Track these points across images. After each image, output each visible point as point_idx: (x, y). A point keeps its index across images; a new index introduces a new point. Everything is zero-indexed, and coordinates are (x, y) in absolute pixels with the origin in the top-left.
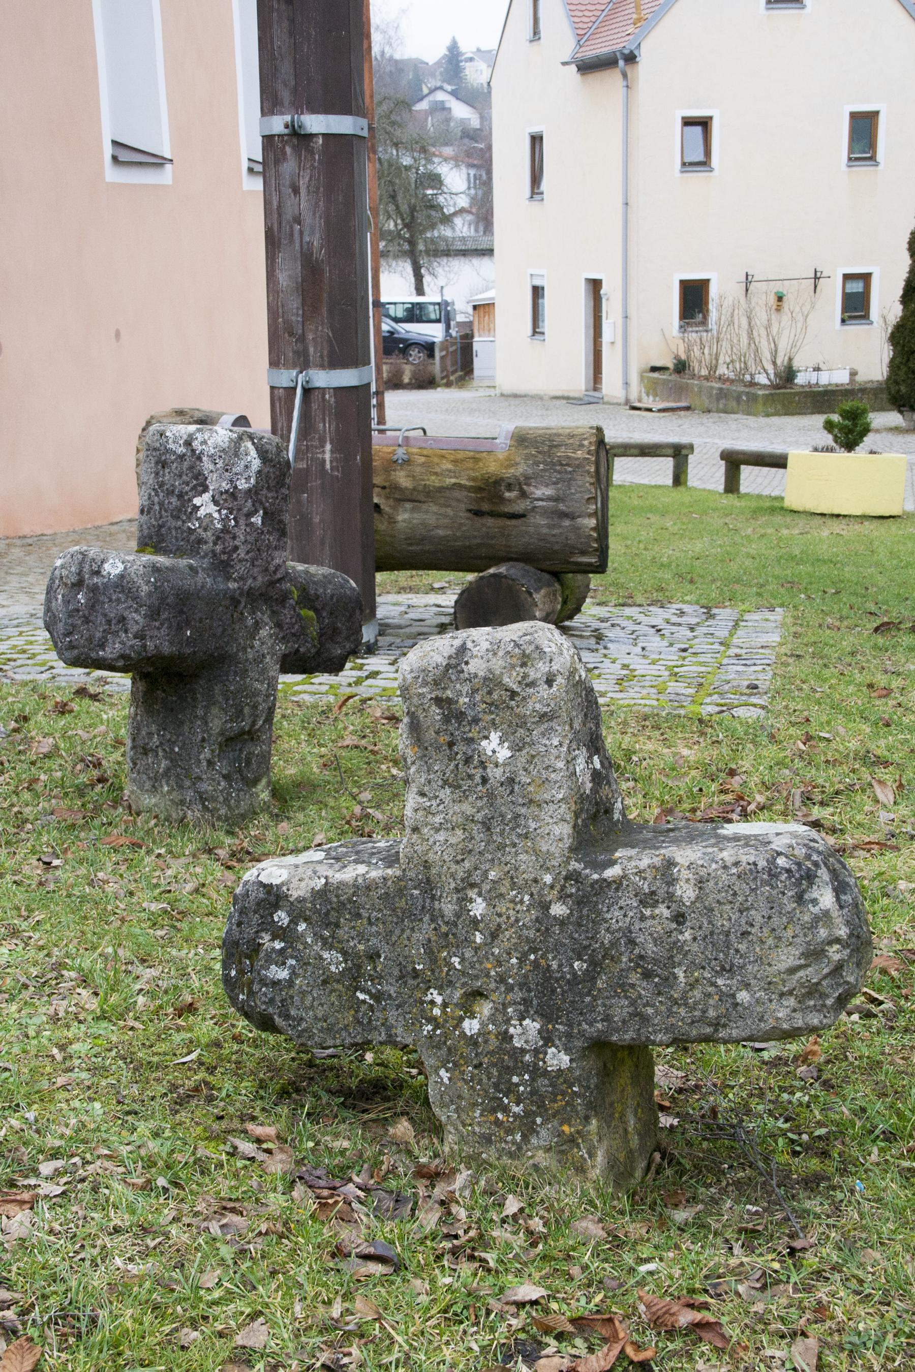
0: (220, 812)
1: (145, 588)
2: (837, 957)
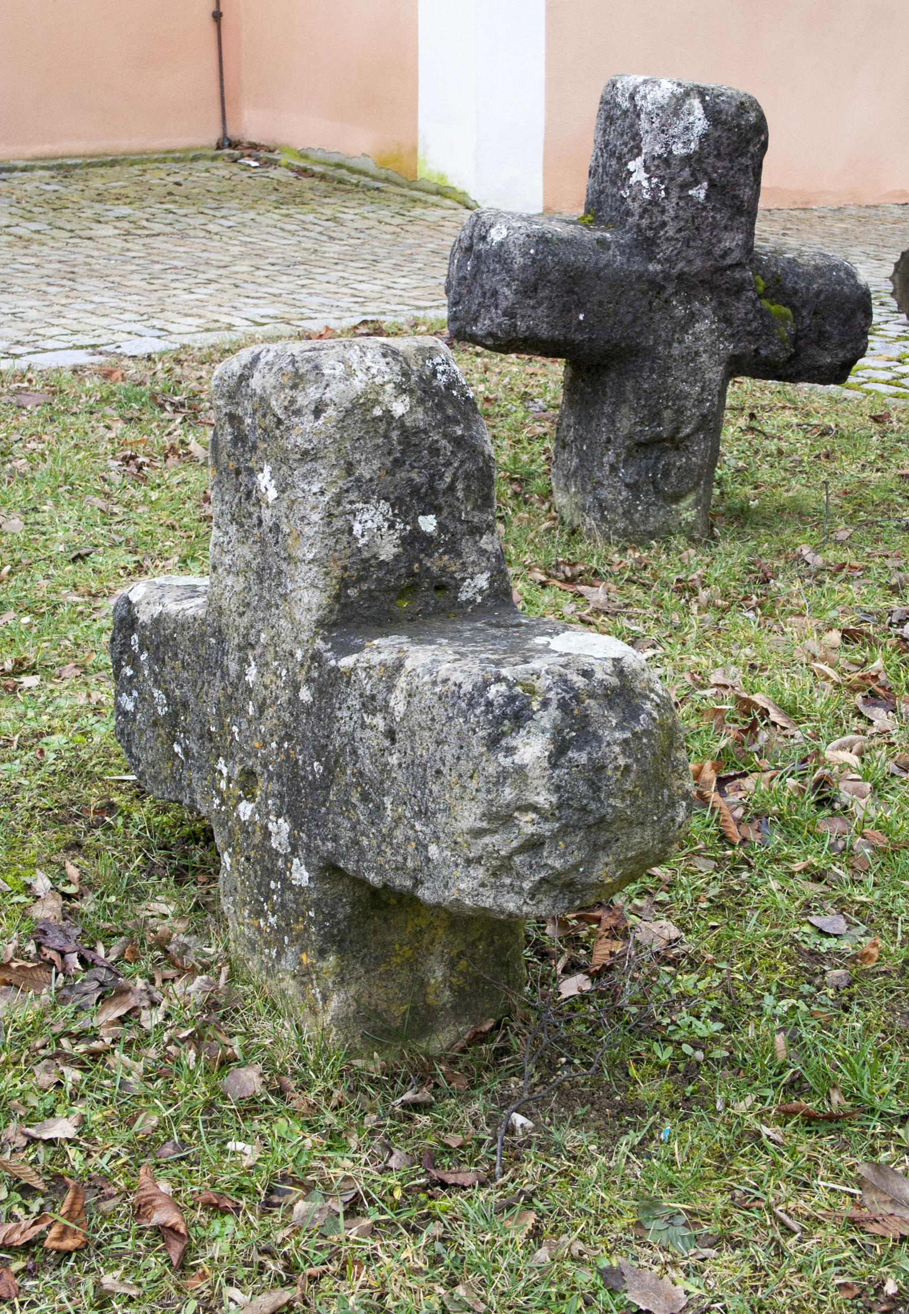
0: (619, 525)
1: (519, 260)
2: (530, 829)
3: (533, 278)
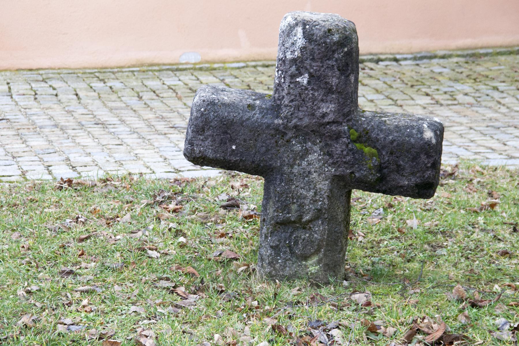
3: (201, 125)
